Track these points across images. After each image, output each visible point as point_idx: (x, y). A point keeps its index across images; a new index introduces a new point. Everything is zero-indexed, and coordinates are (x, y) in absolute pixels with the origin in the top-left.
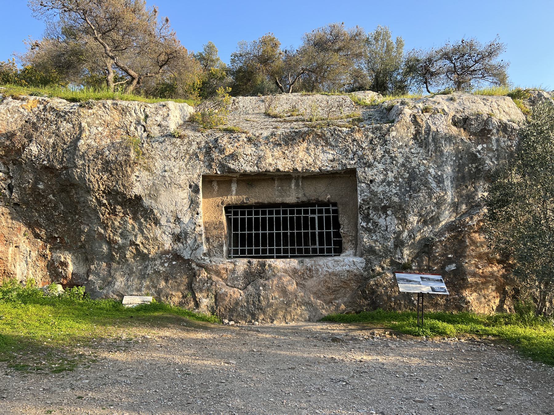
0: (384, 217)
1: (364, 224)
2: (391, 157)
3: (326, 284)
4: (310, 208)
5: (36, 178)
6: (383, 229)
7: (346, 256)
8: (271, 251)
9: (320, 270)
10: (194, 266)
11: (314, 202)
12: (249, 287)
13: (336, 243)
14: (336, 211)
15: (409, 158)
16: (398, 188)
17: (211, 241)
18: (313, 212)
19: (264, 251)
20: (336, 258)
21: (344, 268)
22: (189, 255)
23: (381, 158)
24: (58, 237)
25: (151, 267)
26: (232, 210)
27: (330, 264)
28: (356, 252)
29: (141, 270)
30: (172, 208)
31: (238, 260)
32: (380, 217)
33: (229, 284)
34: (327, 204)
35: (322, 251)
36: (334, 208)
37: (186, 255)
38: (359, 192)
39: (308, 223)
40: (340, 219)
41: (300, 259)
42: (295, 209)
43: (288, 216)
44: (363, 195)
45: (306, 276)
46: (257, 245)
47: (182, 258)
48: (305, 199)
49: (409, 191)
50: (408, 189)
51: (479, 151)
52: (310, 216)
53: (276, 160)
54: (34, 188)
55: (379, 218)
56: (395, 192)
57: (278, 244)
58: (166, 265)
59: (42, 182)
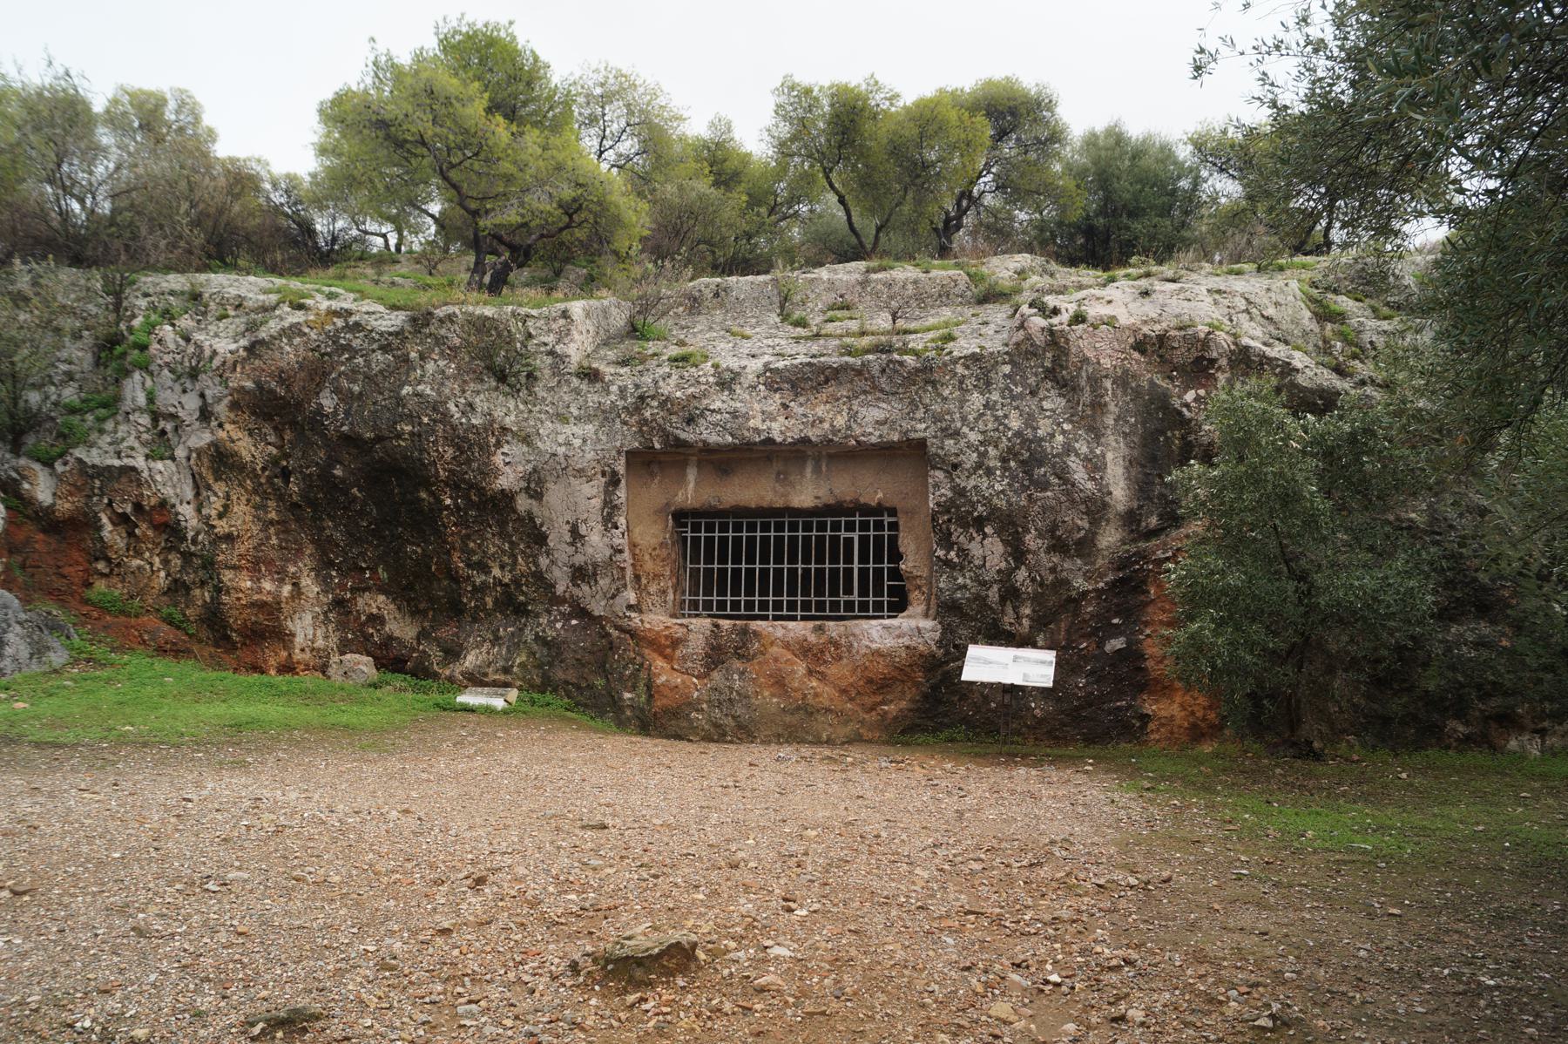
0: (979, 539)
1: (940, 553)
2: (997, 418)
5: (330, 457)
6: (977, 562)
7: (909, 617)
8: (792, 606)
12: (715, 674)
13: (893, 591)
14: (894, 526)
17: (644, 581)
18: (850, 527)
26: (690, 521)
32: (972, 539)
34: (879, 510)
35: (864, 606)
37: (598, 608)
51: (1187, 405)
52: (843, 534)
53: (771, 419)
54: (325, 473)
58: (558, 625)
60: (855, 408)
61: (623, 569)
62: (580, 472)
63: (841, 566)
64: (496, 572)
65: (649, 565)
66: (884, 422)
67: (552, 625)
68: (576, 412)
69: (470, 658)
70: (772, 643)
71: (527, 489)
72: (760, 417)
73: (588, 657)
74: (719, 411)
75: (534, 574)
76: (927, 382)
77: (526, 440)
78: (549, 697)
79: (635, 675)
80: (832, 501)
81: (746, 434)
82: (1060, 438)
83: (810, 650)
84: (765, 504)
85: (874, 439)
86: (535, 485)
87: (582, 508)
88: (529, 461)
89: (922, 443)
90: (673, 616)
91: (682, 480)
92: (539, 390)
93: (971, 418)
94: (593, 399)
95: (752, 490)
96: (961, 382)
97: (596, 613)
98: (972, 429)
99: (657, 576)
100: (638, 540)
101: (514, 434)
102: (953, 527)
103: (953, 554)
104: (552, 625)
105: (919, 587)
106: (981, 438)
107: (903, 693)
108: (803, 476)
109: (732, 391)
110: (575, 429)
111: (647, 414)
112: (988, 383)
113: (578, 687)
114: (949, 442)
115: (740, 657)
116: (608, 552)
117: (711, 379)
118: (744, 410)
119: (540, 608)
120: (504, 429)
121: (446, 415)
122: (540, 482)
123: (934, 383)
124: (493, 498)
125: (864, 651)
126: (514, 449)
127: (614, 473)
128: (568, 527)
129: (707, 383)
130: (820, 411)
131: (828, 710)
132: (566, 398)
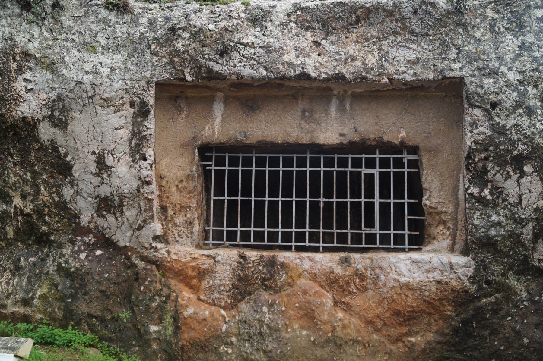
0: (515, 177)
1: (474, 190)
4: (364, 156)
6: (512, 200)
7: (434, 251)
9: (382, 277)
11: (374, 143)
12: (243, 306)
14: (413, 164)
17: (170, 212)
18: (371, 164)
19: (273, 237)
20: (415, 255)
21: (430, 275)
22: (127, 239)
23: (513, 61)
25: (54, 261)
26: (214, 155)
28: (454, 244)
29: (34, 264)
30: (95, 147)
33: (202, 297)
36: (411, 157)
37: (123, 239)
40: (423, 179)
41: (343, 254)
42: (336, 156)
43: (322, 169)
46: (259, 223)
52: (364, 170)
55: (506, 180)
57: (301, 224)
58: (83, 256)
60: (385, 48)
61: (151, 201)
62: (108, 102)
63: (363, 200)
64: (17, 201)
65: (176, 197)
66: (416, 62)
67: (75, 256)
68: (104, 42)
70: (300, 276)
71: (51, 117)
72: (293, 53)
73: (113, 288)
74: (252, 45)
75: (57, 205)
76: (458, 24)
77: (51, 67)
78: (71, 333)
79: (161, 307)
80: (357, 139)
81: (281, 68)
83: (336, 281)
84: (291, 140)
85: (408, 77)
86: (59, 113)
87: (108, 138)
88: (53, 89)
89: (460, 82)
90: (198, 247)
91: (209, 116)
92: (66, 19)
93: (508, 58)
94: (121, 30)
95: (278, 126)
96: (492, 26)
97: (122, 244)
98: (510, 69)
99: (183, 208)
100: (164, 172)
101: (38, 61)
102: (490, 165)
103: (486, 191)
104: (75, 256)
105: (444, 223)
106: (520, 78)
107: (429, 324)
108: (327, 114)
109: (264, 28)
110: (103, 59)
111: (179, 45)
112: (521, 26)
113: (102, 320)
114: (488, 82)
115: (267, 288)
116: (135, 184)
117: (243, 15)
118: (277, 45)
119: (63, 239)
120: (27, 55)
122: (65, 110)
123: (465, 26)
124: (14, 126)
125: (391, 284)
126: (39, 77)
127: (144, 104)
128: (93, 158)
129: (239, 17)
130: (352, 49)
131: (355, 342)
132: (94, 27)
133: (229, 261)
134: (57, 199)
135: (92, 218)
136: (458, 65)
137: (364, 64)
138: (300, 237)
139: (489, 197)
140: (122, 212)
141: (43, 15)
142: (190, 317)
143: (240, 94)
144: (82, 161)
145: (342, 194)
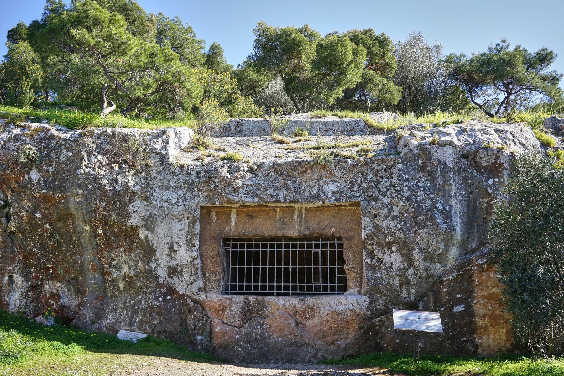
2: (397, 191)
3: (329, 324)
6: (387, 266)
8: (287, 288)
9: (322, 309)
10: (189, 301)
14: (340, 246)
15: (415, 192)
16: (403, 223)
17: (207, 275)
18: (317, 246)
19: (264, 288)
20: (340, 297)
22: (184, 290)
23: (386, 192)
24: (51, 268)
25: (145, 302)
27: (333, 304)
31: (235, 296)
32: (384, 253)
34: (331, 238)
38: (363, 226)
39: (312, 259)
40: (344, 254)
41: (301, 297)
44: (367, 229)
45: (307, 315)
47: (177, 293)
48: (308, 233)
49: (415, 227)
50: (413, 224)
51: (489, 186)
52: (313, 250)
55: (384, 254)
56: (400, 227)
58: (161, 299)
59: (40, 211)
65: (210, 267)
69: (110, 317)
77: (146, 199)
82: (428, 202)
87: (174, 236)
99: (214, 273)
116: (190, 259)
121: (101, 187)
127: (194, 217)
128: (167, 246)
133: (239, 301)
134: (147, 268)
135: (166, 278)
136: (358, 194)
137: (310, 193)
138: (279, 288)
139: (377, 264)
140: (182, 275)
141: (141, 171)
142: (218, 331)
143: (245, 209)
144: (161, 247)
145: (301, 264)
